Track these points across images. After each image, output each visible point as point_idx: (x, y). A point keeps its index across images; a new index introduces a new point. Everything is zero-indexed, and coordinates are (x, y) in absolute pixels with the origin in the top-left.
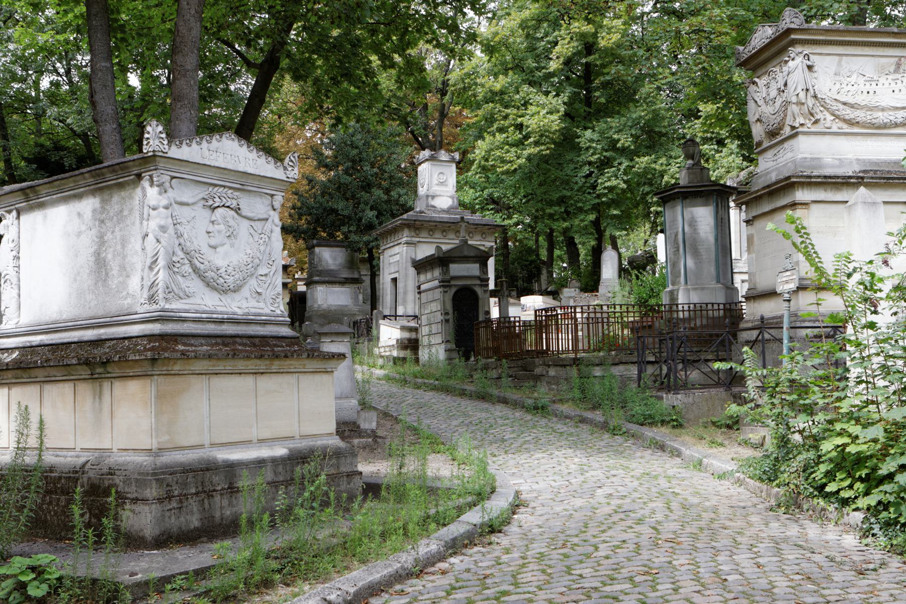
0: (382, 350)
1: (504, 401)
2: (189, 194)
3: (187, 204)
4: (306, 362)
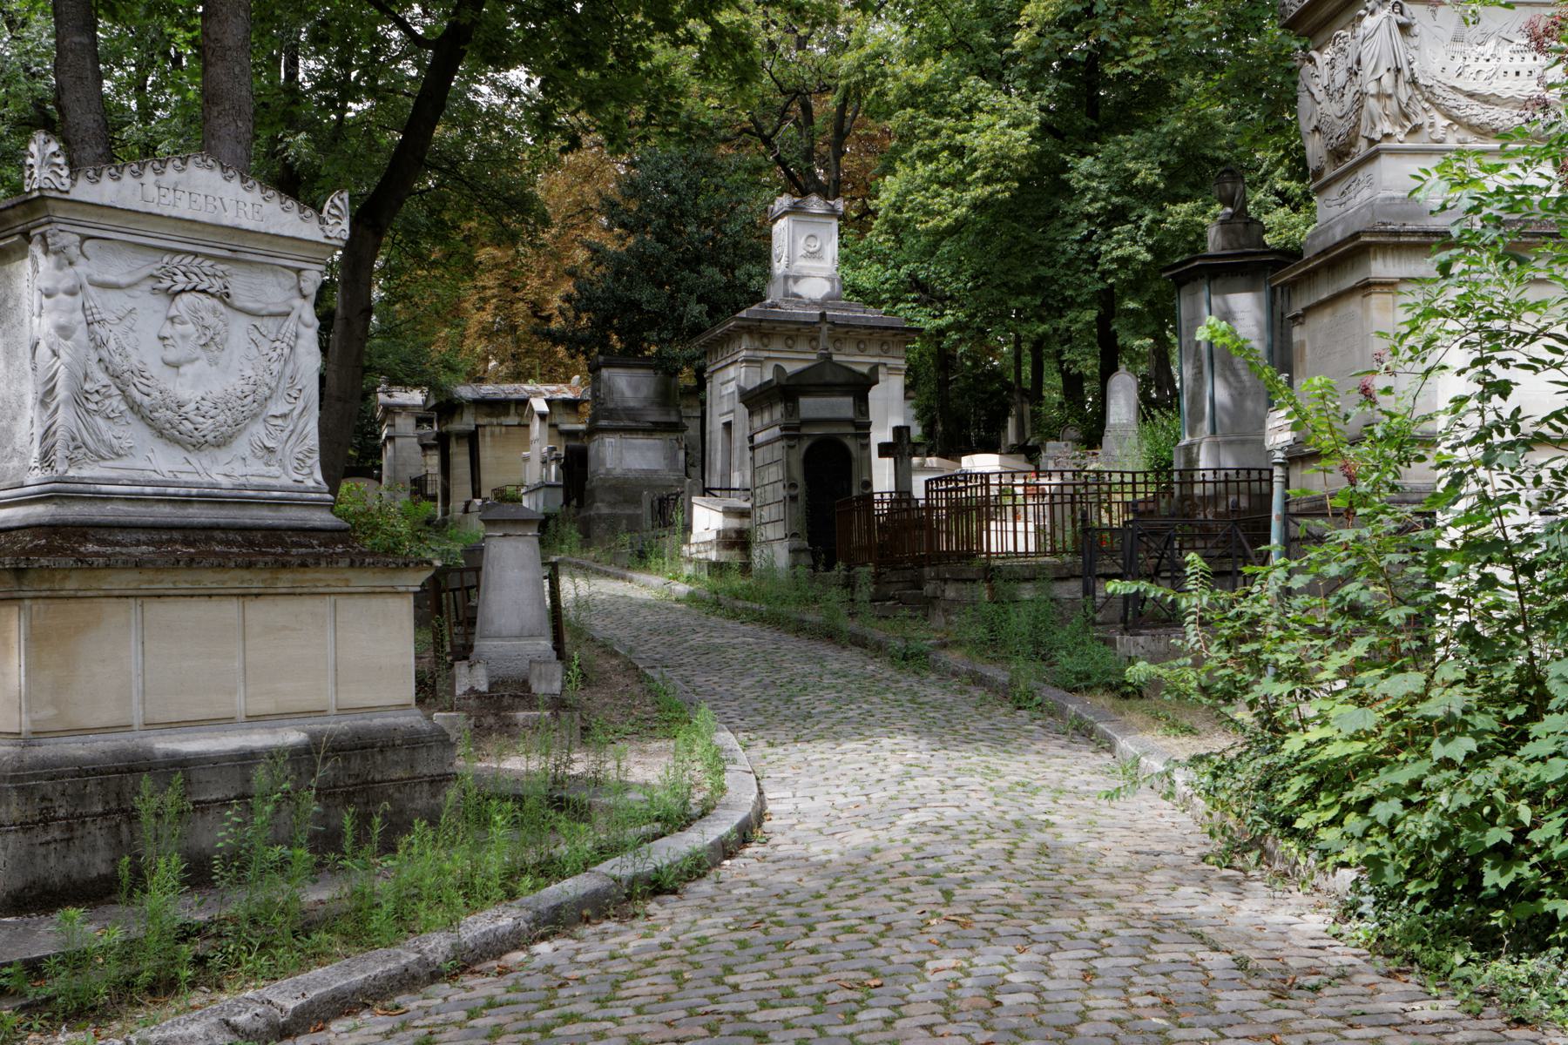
0: (693, 549)
1: (859, 642)
2: (118, 269)
3: (117, 287)
4: (350, 574)
